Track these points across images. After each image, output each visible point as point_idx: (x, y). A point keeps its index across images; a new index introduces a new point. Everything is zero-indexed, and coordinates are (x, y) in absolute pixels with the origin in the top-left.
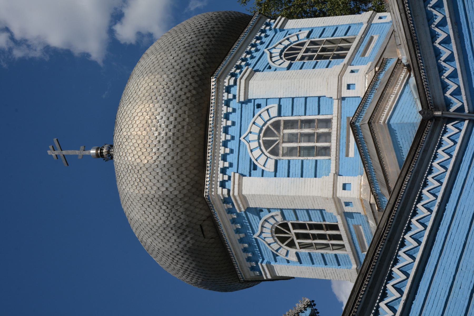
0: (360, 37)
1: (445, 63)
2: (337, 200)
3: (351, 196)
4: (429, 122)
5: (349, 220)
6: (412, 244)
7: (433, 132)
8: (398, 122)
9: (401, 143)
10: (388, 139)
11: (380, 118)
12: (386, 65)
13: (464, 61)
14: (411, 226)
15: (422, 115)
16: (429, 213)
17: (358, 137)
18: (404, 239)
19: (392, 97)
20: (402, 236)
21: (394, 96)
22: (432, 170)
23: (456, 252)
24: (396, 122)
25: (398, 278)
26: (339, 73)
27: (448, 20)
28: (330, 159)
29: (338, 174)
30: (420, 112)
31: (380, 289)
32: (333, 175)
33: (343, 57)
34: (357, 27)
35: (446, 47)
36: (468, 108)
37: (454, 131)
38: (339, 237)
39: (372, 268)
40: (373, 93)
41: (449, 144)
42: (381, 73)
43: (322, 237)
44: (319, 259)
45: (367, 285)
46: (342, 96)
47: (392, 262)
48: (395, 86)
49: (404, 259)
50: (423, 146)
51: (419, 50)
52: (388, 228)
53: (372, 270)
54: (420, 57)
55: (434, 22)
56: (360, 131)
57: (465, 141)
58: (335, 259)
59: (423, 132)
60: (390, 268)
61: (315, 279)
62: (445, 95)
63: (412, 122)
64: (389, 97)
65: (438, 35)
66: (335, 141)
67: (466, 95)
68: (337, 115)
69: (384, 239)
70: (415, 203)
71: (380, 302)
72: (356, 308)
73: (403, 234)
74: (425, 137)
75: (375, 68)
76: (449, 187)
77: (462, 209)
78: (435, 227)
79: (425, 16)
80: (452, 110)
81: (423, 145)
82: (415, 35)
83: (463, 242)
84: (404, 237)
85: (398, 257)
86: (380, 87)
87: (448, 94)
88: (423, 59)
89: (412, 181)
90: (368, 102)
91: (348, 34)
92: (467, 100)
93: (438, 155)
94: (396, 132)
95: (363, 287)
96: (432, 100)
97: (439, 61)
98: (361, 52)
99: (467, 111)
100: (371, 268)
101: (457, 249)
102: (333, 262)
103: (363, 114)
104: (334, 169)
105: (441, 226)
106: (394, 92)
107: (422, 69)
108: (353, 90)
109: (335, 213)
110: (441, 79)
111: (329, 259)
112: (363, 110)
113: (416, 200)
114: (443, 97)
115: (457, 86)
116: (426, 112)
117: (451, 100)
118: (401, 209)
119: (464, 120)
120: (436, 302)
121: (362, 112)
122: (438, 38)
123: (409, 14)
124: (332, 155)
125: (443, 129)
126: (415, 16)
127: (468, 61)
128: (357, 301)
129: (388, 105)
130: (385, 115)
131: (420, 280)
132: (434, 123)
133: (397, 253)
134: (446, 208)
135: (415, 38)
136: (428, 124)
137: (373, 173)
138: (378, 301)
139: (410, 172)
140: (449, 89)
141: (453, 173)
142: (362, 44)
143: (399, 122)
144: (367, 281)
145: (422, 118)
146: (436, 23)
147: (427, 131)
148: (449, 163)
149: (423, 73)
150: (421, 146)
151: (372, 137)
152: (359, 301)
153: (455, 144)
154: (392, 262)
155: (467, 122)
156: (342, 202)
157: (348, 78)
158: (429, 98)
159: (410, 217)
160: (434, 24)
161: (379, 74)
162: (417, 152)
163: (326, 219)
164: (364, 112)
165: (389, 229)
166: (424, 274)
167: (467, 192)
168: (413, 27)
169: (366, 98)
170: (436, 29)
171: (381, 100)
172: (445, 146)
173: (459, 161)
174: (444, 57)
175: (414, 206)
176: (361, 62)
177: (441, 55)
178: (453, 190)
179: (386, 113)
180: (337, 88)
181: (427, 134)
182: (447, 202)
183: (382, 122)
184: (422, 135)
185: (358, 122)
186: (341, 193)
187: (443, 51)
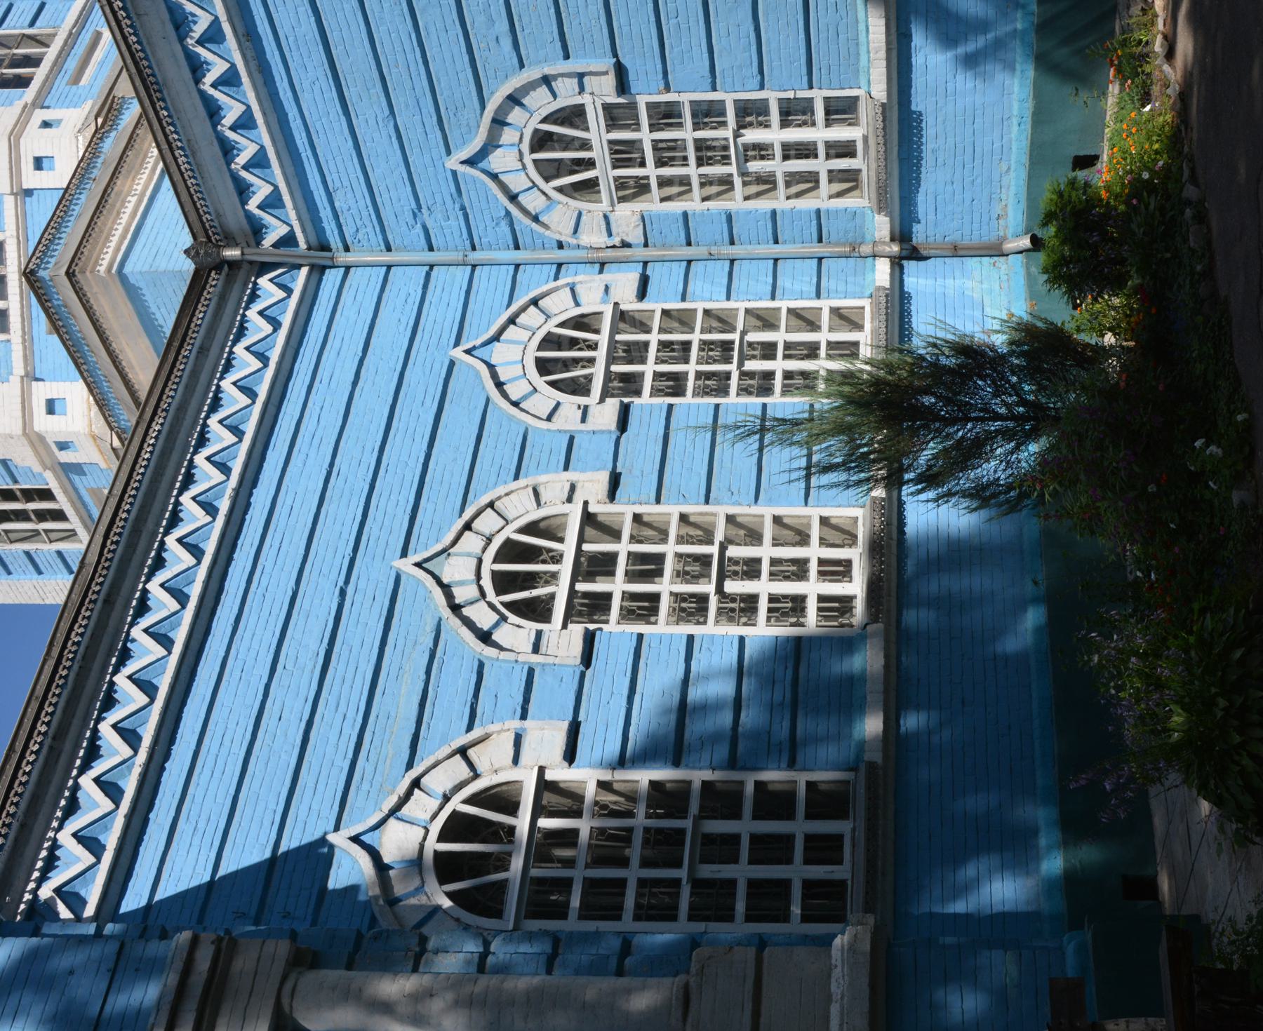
0: (67, 33)
1: (235, 132)
2: (36, 441)
3: (70, 429)
4: (213, 274)
5: (76, 478)
6: (165, 606)
7: (223, 298)
8: (144, 270)
9: (158, 316)
10: (126, 308)
11: (98, 258)
12: (121, 114)
13: (281, 128)
14: (164, 555)
15: (192, 259)
16: (209, 519)
17: (50, 305)
18: (145, 592)
19: (129, 202)
20: (141, 586)
21: (134, 200)
22: (221, 399)
23: (272, 620)
24: (138, 268)
25: (128, 704)
26: (9, 129)
27: (227, 28)
28: (9, 341)
29: (31, 376)
30: (187, 252)
31: (80, 736)
32: (19, 379)
33: (23, 82)
34: (60, 6)
35: (231, 93)
36: (306, 237)
37: (273, 295)
38: (59, 516)
39: (58, 686)
40: (84, 189)
41: (261, 330)
42: (107, 137)
43: (21, 516)
44: (20, 562)
45: (45, 734)
46: (25, 186)
47: (114, 660)
48: (138, 173)
49: (145, 650)
50: (195, 338)
51: (163, 100)
52: (104, 568)
53: (57, 692)
54: (167, 119)
55: (191, 30)
56: (54, 290)
57: (301, 320)
58: (59, 561)
59: (198, 302)
60: (108, 676)
61: (21, 605)
62: (246, 207)
63: (177, 269)
64: (124, 202)
65: (208, 64)
66: (18, 298)
67: (296, 208)
68: (15, 234)
69: (91, 601)
70: (175, 492)
71: (79, 774)
72: (12, 803)
73: (143, 579)
74: (202, 316)
75: (96, 119)
76: (259, 446)
77: (289, 502)
78: (223, 555)
79: (166, 16)
80: (268, 241)
81: (196, 338)
82: (145, 63)
83: (290, 593)
84: (147, 586)
85: (129, 645)
86: (101, 173)
87: (252, 206)
88: (177, 122)
89: (170, 432)
90: (72, 215)
91: (38, 23)
92: (299, 219)
93: (234, 358)
94: (143, 292)
95: (32, 742)
96: (216, 221)
97: (219, 127)
98: (69, 73)
99: (302, 244)
100: (55, 685)
101: (275, 611)
102: (54, 567)
103: (58, 247)
104: (21, 364)
105: (238, 550)
106: (136, 190)
107: (179, 148)
108: (51, 172)
109: (37, 468)
110: (230, 170)
111: (45, 562)
112: (58, 236)
113: (178, 485)
114: (242, 213)
115: (272, 188)
116: (202, 252)
117: (262, 219)
118: (139, 510)
119: (299, 267)
120: (220, 762)
121: (57, 241)
122: (209, 70)
123: (120, 9)
124: (12, 332)
125: (249, 291)
126: (138, 15)
127: (290, 128)
128: (17, 782)
129: (120, 224)
130: (110, 250)
131: (183, 703)
132: (228, 275)
133: (128, 633)
134: (252, 500)
135: (148, 70)
136: (211, 279)
137: (105, 384)
138: (75, 772)
139: (163, 410)
140: (254, 193)
141: (270, 406)
142: (73, 52)
143: (146, 268)
144: (43, 722)
145: (193, 266)
146: (196, 35)
147: (206, 299)
148: (261, 381)
149: (183, 158)
150: (191, 338)
151: (84, 306)
152: (21, 783)
153: (275, 330)
154: (114, 660)
155: (305, 270)
156: (50, 441)
157: (35, 142)
158: (207, 216)
159: (161, 530)
160: (192, 38)
161: (101, 139)
162: (180, 357)
163: (19, 479)
164: (61, 241)
165: (105, 572)
166: (195, 684)
167: (302, 456)
168: (139, 42)
169: (68, 203)
170: (199, 50)
171: (101, 212)
172: (251, 336)
173: (284, 373)
174: (229, 118)
175: (172, 500)
176: (68, 100)
177: (222, 114)
178: (269, 452)
179: (113, 245)
180: (7, 166)
181: (207, 306)
182: (254, 484)
183: (102, 269)
184: (196, 308)
185: (45, 269)
186: (43, 423)
187: (225, 103)
